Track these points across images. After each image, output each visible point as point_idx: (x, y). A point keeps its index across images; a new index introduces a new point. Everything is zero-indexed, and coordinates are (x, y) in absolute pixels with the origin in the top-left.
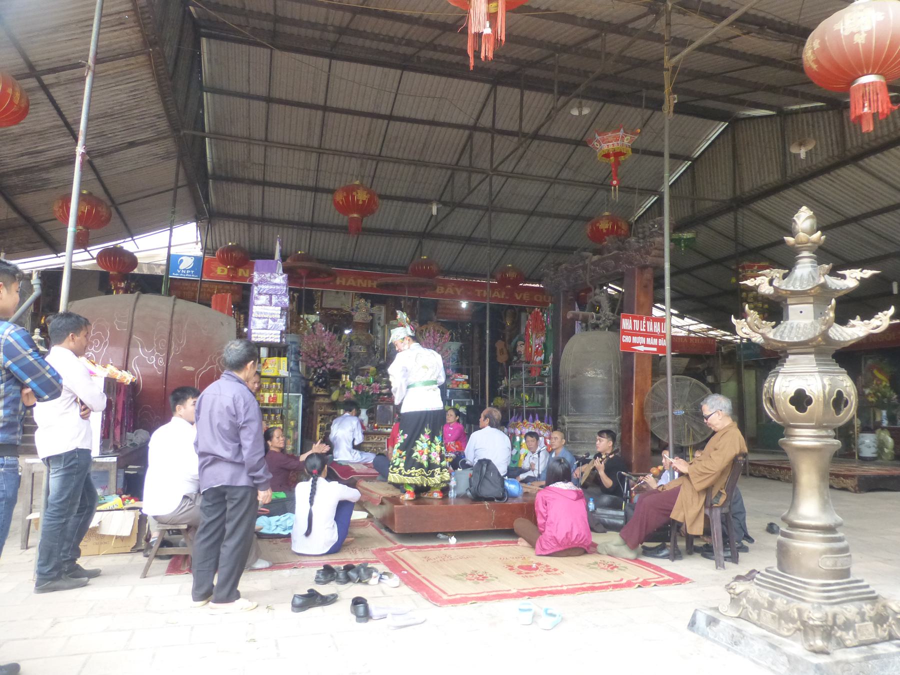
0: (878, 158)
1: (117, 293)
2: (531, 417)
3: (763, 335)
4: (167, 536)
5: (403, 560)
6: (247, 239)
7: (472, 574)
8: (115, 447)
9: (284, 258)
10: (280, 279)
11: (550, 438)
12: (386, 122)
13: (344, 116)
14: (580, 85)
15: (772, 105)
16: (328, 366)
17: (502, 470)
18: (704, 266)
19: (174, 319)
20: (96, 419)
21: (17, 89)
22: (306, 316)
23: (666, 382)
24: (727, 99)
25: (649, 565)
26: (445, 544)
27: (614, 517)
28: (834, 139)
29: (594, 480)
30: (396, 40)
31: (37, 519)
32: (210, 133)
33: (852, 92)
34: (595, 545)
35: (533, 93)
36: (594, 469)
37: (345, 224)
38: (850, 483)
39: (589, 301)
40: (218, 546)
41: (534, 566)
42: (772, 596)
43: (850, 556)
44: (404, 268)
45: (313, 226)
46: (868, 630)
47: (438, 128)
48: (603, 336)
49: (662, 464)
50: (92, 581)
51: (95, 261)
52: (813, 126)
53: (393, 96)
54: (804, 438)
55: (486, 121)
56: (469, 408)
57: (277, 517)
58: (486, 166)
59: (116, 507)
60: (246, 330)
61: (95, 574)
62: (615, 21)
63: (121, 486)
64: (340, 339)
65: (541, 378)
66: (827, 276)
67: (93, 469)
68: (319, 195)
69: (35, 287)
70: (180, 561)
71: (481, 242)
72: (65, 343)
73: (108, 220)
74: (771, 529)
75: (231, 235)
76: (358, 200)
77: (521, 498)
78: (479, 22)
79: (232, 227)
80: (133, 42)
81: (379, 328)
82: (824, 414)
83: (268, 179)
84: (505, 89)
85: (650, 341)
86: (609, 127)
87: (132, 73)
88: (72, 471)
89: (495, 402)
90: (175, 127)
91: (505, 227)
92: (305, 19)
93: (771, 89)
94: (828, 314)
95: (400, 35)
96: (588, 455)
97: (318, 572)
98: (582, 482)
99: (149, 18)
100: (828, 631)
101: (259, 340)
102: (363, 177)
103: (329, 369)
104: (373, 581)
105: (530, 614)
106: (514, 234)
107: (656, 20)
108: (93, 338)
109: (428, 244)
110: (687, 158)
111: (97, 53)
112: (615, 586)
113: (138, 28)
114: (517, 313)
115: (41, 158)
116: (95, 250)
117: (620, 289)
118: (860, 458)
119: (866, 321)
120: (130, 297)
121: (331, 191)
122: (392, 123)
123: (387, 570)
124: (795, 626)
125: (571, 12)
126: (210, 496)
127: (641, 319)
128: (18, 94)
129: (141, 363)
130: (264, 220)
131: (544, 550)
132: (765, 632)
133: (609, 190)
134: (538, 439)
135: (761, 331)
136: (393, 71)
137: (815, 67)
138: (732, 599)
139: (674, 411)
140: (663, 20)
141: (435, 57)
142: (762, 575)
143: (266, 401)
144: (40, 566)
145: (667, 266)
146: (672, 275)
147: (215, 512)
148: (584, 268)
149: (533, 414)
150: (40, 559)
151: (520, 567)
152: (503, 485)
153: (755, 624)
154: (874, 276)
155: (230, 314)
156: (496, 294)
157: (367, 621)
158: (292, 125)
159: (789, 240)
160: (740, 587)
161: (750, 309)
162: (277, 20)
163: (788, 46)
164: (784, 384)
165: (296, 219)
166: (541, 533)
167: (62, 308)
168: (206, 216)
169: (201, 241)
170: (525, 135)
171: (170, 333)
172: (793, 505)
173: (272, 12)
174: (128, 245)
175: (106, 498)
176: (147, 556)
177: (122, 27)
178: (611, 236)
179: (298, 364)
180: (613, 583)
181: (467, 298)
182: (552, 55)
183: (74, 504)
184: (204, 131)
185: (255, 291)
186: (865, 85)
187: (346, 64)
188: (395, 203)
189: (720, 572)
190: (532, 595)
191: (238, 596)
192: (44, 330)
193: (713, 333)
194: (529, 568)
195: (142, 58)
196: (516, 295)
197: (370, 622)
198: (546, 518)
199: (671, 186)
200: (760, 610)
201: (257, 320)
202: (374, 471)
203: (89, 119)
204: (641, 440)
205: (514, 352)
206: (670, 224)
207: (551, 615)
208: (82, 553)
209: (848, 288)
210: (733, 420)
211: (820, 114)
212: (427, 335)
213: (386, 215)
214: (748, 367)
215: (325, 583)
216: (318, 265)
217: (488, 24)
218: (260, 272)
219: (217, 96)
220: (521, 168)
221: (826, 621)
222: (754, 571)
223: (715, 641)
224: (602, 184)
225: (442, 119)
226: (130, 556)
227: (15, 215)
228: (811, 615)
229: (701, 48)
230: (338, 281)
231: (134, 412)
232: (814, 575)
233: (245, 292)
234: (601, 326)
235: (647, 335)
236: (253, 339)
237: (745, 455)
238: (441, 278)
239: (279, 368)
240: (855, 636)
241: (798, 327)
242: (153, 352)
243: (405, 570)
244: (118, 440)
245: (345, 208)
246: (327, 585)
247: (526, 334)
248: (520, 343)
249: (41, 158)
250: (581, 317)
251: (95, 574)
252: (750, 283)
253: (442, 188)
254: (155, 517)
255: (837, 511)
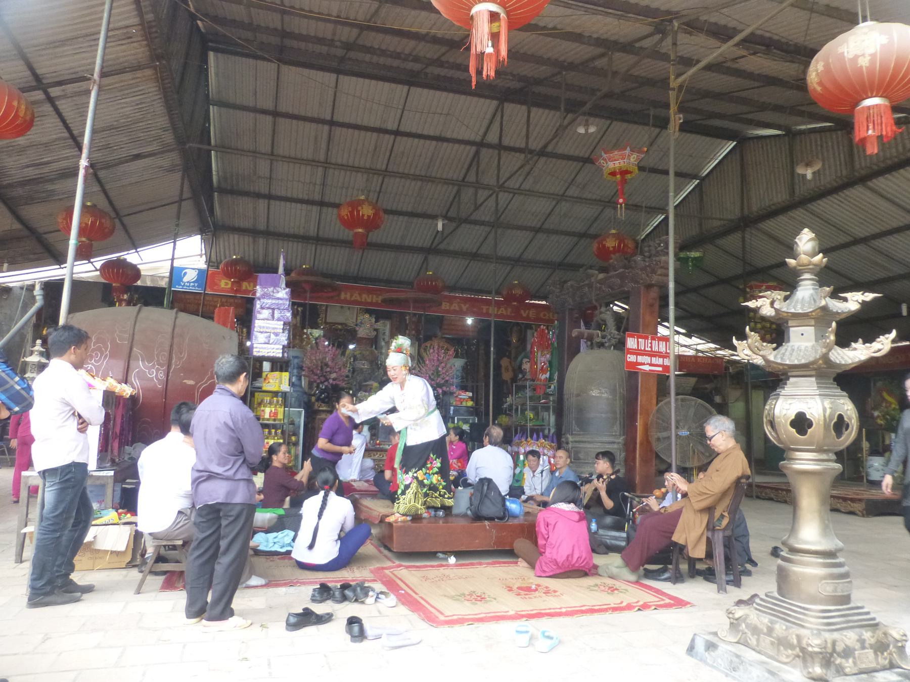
0: (887, 179)
1: (120, 305)
2: (535, 436)
3: (763, 357)
4: (162, 551)
5: (400, 579)
6: (252, 253)
7: (471, 595)
8: (113, 461)
9: (287, 272)
10: (283, 293)
11: (554, 457)
12: (393, 137)
13: (350, 131)
14: (585, 103)
15: (768, 124)
16: (331, 381)
17: (504, 489)
18: (712, 285)
19: (176, 332)
20: (94, 433)
21: (23, 102)
22: (309, 331)
23: (669, 402)
24: (735, 118)
25: (650, 588)
26: (444, 563)
27: (616, 538)
28: (842, 159)
29: (596, 499)
30: (403, 56)
31: (32, 533)
32: (216, 146)
33: (856, 115)
34: (596, 567)
35: (541, 110)
36: (596, 489)
37: (351, 238)
38: (857, 507)
39: (595, 319)
40: (210, 564)
41: (534, 587)
42: (772, 622)
43: (850, 582)
44: (410, 284)
45: (319, 240)
46: (868, 658)
47: (445, 144)
48: (609, 355)
49: (665, 487)
50: (85, 596)
51: (98, 273)
52: (822, 146)
53: (399, 112)
54: (805, 461)
55: (492, 138)
56: (472, 426)
57: (275, 534)
58: (493, 182)
59: (111, 522)
60: (248, 344)
61: (89, 589)
62: (622, 40)
63: (117, 500)
64: (343, 354)
65: (547, 396)
66: (828, 299)
67: (89, 482)
68: (325, 209)
69: (38, 298)
70: (175, 578)
71: (486, 258)
72: (65, 356)
73: (112, 232)
74: (775, 552)
75: (236, 248)
76: (363, 215)
77: (522, 517)
78: (482, 41)
79: (236, 240)
80: (140, 56)
81: (383, 344)
82: (824, 438)
83: (273, 192)
84: (512, 105)
85: (655, 360)
86: (617, 146)
87: (138, 86)
88: (68, 484)
89: (499, 419)
90: (181, 141)
91: (512, 244)
92: (312, 34)
93: (778, 108)
94: (828, 337)
95: (407, 52)
96: (591, 475)
97: (314, 590)
98: (585, 502)
99: (156, 32)
100: (827, 658)
101: (261, 354)
102: (369, 191)
103: (332, 385)
104: (370, 600)
105: (527, 636)
106: (521, 251)
107: (662, 40)
108: (93, 350)
109: (434, 260)
110: (695, 177)
111: (102, 67)
112: (615, 609)
113: (145, 42)
114: (523, 330)
115: (46, 170)
116: (99, 262)
117: (627, 307)
118: (868, 481)
119: (867, 345)
120: (133, 310)
121: (337, 206)
122: (399, 138)
123: (384, 589)
124: (794, 652)
125: (578, 31)
126: (204, 512)
127: (646, 338)
128: (23, 107)
129: (141, 376)
130: (269, 234)
131: (544, 571)
132: (763, 658)
133: (615, 208)
134: (539, 458)
135: (761, 353)
136: (400, 86)
137: (819, 89)
138: (731, 624)
139: (677, 432)
140: (669, 40)
141: (442, 74)
142: (762, 600)
143: (267, 416)
144: (33, 580)
145: (671, 285)
146: (677, 294)
147: (209, 528)
148: (590, 286)
149: (537, 432)
150: (33, 574)
151: (520, 588)
152: (504, 505)
153: (754, 650)
154: (875, 299)
155: (232, 328)
156: (502, 311)
157: (362, 641)
158: (299, 139)
159: (791, 262)
160: (740, 612)
161: (751, 330)
162: (285, 34)
163: (795, 66)
164: (785, 406)
165: (302, 232)
166: (541, 554)
167: (62, 321)
168: (210, 228)
169: (206, 254)
170: (531, 152)
171: (171, 346)
172: (793, 529)
173: (279, 27)
174: (132, 257)
175: (103, 512)
176: (141, 572)
177: (129, 41)
178: (617, 255)
179: (300, 379)
180: (613, 606)
181: (472, 314)
182: (559, 73)
183: (67, 519)
184: (209, 143)
185: (258, 305)
186: (869, 108)
187: (354, 79)
188: (401, 218)
189: (721, 596)
190: (530, 616)
191: (232, 613)
192: (45, 343)
193: (721, 353)
194: (528, 589)
195: (148, 72)
196: (522, 312)
197: (365, 643)
198: (546, 540)
199: (676, 207)
200: (759, 636)
201: (259, 334)
202: (375, 489)
203: (94, 132)
204: (645, 461)
205: (519, 369)
206: (675, 243)
207: (549, 637)
208: (77, 567)
209: (850, 311)
210: (737, 442)
211: (828, 134)
212: (431, 351)
213: (392, 230)
214: (756, 387)
215: (321, 602)
216: (321, 279)
217: (490, 44)
218: (263, 287)
219: (224, 110)
220: (527, 185)
221: (825, 648)
222: (755, 596)
223: (712, 666)
224: (609, 202)
225: (448, 135)
226: (124, 572)
227: (17, 226)
228: (810, 642)
229: (709, 68)
230: (343, 296)
231: (131, 424)
232: (814, 600)
233: (249, 306)
234: (607, 345)
235: (652, 354)
236: (255, 354)
237: (748, 478)
238: (446, 293)
239: (281, 383)
240: (855, 663)
241: (799, 349)
242: (154, 365)
243: (402, 589)
244: (116, 452)
245: (351, 222)
246: (323, 604)
247: (532, 352)
248: (525, 360)
249: (46, 170)
250: (586, 335)
251: (89, 589)
252: (752, 304)
253: (448, 203)
254: (150, 534)
255: (838, 536)
